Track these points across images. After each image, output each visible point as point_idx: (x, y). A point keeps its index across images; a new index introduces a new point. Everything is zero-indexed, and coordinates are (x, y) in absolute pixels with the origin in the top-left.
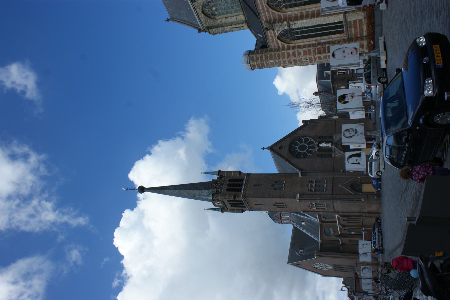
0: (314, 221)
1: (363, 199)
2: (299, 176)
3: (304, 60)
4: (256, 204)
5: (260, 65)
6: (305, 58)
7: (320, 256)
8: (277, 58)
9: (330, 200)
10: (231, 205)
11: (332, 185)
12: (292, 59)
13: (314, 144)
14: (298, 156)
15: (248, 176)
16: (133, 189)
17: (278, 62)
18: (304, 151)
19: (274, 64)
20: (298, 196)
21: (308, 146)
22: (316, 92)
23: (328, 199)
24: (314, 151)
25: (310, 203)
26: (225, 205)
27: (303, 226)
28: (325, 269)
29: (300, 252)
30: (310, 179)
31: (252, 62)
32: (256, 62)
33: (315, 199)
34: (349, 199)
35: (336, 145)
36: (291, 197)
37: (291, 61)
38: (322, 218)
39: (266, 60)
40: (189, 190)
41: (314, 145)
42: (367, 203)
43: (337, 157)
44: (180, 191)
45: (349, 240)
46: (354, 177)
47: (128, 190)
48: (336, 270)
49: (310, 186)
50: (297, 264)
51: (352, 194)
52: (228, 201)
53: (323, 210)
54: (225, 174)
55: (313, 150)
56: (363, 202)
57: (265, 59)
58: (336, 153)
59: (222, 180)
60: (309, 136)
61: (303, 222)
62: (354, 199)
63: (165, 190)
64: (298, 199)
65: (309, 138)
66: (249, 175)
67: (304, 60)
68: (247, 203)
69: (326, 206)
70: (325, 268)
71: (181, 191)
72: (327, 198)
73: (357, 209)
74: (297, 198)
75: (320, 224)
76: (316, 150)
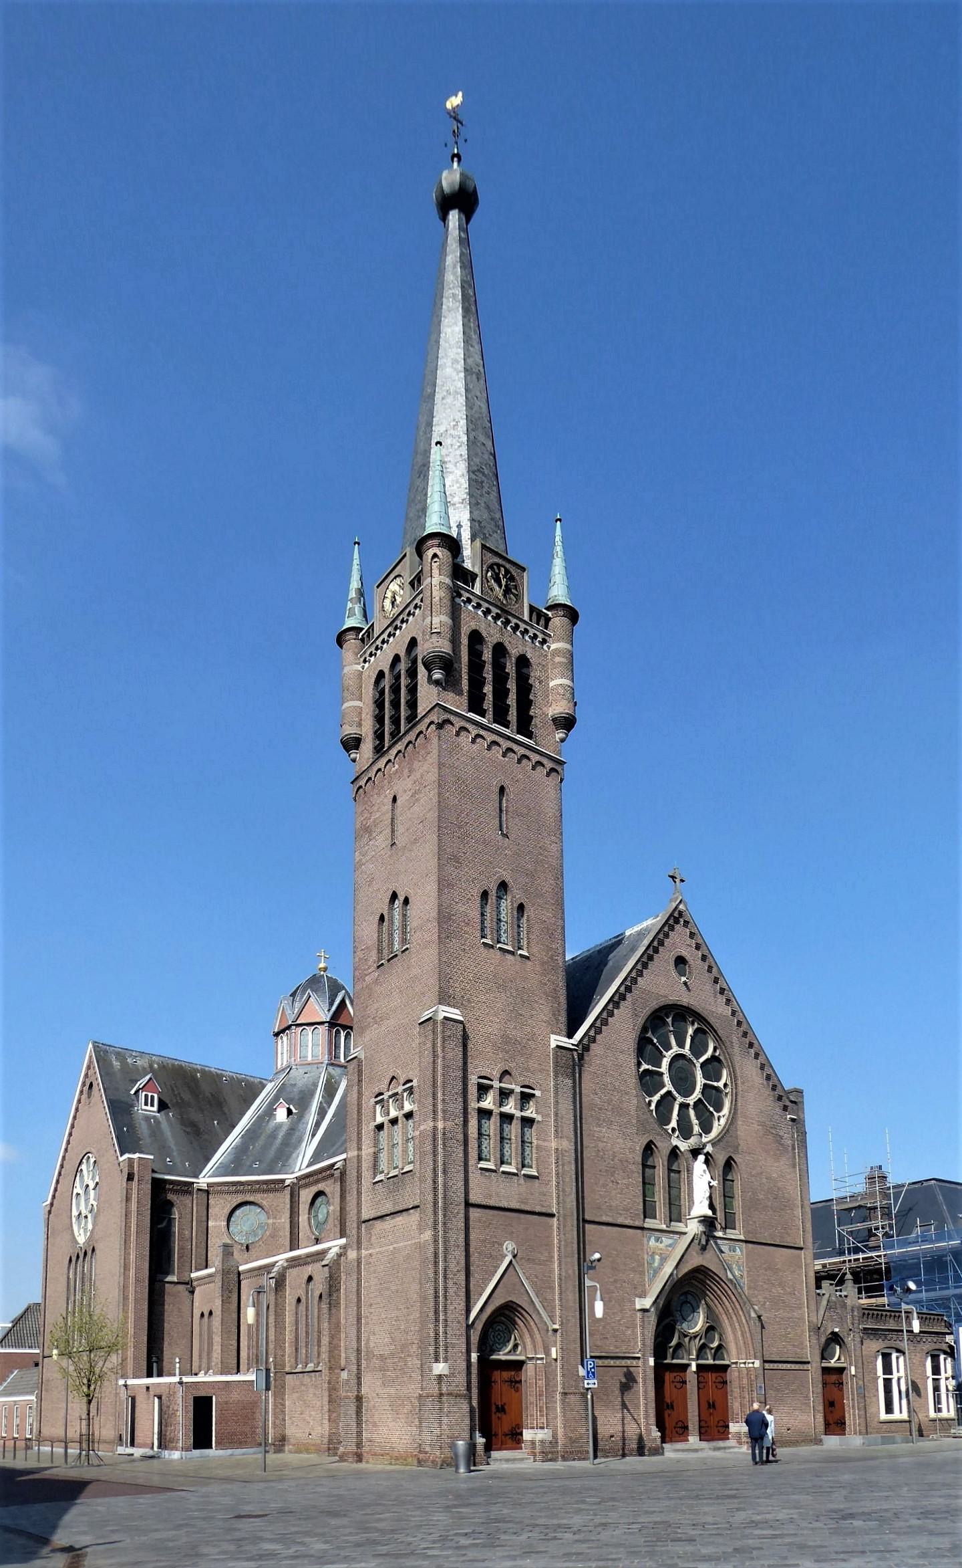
0: (294, 1155)
1: (446, 1372)
4: (395, 799)
7: (130, 1177)
9: (435, 1189)
10: (387, 671)
14: (645, 1048)
15: (549, 765)
18: (666, 1079)
21: (692, 1103)
22: (883, 1178)
23: (440, 1180)
24: (670, 1131)
25: (415, 1083)
26: (385, 636)
27: (270, 1112)
28: (75, 1213)
29: (150, 1094)
30: (537, 1093)
33: (440, 1107)
34: (441, 1293)
35: (704, 1242)
38: (314, 1189)
40: (464, 438)
42: (420, 1396)
43: (645, 1242)
44: (457, 393)
45: (211, 1313)
46: (556, 1327)
49: (503, 1085)
50: (91, 1085)
51: (468, 1311)
53: (366, 1165)
54: (559, 641)
55: (674, 1124)
56: (424, 1370)
58: (666, 1240)
59: (526, 618)
61: (290, 1112)
62: (446, 1320)
63: (460, 318)
64: (436, 1011)
65: (726, 1111)
66: (553, 770)
70: (80, 1214)
71: (462, 400)
72: (445, 1172)
73: (378, 1339)
74: (442, 1007)
75: (283, 1181)
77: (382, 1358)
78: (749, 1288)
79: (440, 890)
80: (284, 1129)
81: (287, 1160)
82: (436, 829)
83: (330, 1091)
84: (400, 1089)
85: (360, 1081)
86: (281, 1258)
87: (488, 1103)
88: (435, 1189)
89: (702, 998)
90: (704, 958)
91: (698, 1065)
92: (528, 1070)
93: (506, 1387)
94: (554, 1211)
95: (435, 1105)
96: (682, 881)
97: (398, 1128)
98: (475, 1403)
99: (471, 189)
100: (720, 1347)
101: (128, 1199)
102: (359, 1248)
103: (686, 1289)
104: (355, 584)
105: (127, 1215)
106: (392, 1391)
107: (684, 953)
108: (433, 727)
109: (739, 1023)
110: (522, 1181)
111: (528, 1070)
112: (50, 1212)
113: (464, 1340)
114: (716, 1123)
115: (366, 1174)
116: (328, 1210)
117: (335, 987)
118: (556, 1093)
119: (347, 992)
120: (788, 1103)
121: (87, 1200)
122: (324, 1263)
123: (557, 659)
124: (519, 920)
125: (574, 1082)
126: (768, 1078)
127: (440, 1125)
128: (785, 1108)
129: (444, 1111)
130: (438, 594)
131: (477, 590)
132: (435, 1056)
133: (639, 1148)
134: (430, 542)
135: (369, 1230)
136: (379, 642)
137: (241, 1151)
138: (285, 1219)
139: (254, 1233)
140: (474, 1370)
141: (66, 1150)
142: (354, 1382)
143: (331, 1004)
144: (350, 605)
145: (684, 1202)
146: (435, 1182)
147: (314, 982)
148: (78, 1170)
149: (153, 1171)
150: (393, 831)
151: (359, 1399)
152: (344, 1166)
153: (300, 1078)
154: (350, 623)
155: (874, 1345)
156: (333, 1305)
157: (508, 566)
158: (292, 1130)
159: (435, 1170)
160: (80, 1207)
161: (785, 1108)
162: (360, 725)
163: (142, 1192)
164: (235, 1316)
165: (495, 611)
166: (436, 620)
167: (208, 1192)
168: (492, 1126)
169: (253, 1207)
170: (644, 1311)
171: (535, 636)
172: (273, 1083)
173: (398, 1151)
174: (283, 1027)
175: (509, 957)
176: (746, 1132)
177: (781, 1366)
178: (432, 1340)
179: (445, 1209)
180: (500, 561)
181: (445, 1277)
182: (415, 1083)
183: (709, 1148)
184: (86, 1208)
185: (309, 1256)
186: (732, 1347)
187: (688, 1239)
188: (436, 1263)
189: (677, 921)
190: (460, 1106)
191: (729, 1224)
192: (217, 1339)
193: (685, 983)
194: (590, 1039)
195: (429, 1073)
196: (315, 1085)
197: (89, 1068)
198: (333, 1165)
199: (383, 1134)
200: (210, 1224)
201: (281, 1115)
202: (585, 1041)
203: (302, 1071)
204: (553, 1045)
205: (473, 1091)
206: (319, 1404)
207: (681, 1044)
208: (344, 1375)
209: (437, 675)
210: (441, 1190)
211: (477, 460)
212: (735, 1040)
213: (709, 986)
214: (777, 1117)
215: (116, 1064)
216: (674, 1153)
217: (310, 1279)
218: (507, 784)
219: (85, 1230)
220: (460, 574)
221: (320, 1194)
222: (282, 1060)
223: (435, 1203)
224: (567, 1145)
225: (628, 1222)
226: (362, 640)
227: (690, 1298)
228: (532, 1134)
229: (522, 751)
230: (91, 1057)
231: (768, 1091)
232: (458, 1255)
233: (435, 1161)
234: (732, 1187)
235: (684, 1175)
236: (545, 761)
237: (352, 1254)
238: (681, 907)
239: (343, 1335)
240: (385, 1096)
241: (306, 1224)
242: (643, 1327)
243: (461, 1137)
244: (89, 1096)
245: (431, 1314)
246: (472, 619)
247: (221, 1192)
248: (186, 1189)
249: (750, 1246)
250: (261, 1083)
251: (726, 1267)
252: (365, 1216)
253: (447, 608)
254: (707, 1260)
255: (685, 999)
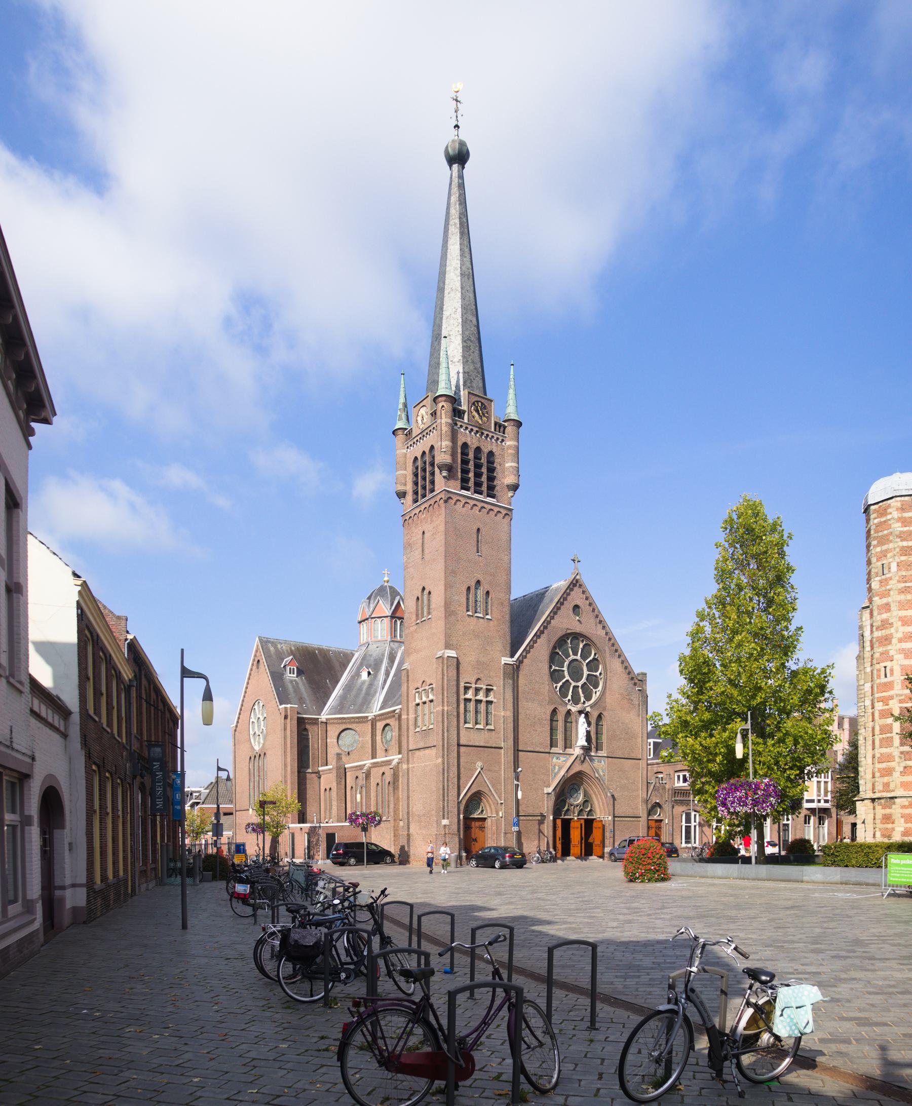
0: (373, 701)
1: (448, 824)
2: (503, 656)
3: (885, 667)
5: (886, 532)
6: (892, 671)
7: (286, 717)
8: (903, 585)
9: (443, 739)
10: (427, 452)
11: (482, 744)
12: (892, 630)
13: (584, 703)
14: (553, 657)
15: (504, 512)
16: (444, 172)
17: (888, 587)
18: (566, 673)
19: (883, 577)
20: (453, 653)
23: (446, 734)
25: (434, 686)
26: (418, 438)
27: (358, 674)
28: (252, 732)
30: (495, 688)
31: (899, 504)
32: (896, 517)
33: (445, 700)
34: (446, 788)
36: (448, 636)
37: (886, 628)
38: (384, 723)
39: (898, 550)
40: (460, 320)
41: (582, 701)
45: (330, 789)
47: (459, 99)
48: (250, 758)
49: (477, 686)
50: (259, 661)
51: (459, 795)
52: (432, 447)
53: (411, 722)
56: (438, 823)
57: (903, 547)
58: (562, 759)
59: (493, 430)
60: (604, 688)
61: (369, 673)
64: (444, 653)
65: (600, 688)
67: (885, 667)
68: (427, 506)
69: (424, 728)
71: (459, 295)
72: (448, 731)
73: (417, 807)
74: (447, 651)
75: (367, 717)
76: (569, 707)
77: (419, 816)
78: (608, 781)
79: (446, 590)
80: (367, 684)
81: (369, 704)
82: (443, 557)
83: (392, 659)
84: (427, 688)
85: (408, 681)
86: (368, 762)
87: (470, 695)
88: (443, 739)
89: (587, 626)
90: (590, 604)
91: (585, 664)
92: (490, 677)
93: (477, 830)
94: (502, 746)
95: (443, 699)
96: (579, 561)
97: (426, 705)
98: (462, 837)
99: (465, 151)
100: (591, 810)
101: (285, 729)
102: (408, 763)
103: (574, 782)
104: (402, 400)
105: (285, 738)
106: (424, 832)
107: (578, 603)
108: (442, 501)
109: (610, 639)
110: (486, 732)
111: (490, 677)
112: (235, 731)
113: (456, 809)
114: (594, 695)
115: (411, 727)
116: (392, 734)
117: (394, 593)
118: (504, 688)
119: (401, 597)
120: (637, 681)
121: (259, 726)
122: (391, 767)
123: (510, 451)
124: (486, 599)
125: (514, 681)
126: (626, 668)
127: (446, 708)
128: (635, 684)
129: (448, 702)
130: (445, 429)
131: (466, 420)
132: (443, 675)
133: (549, 712)
134: (440, 399)
135: (412, 755)
136: (415, 440)
137: (343, 698)
138: (368, 738)
139: (352, 745)
140: (462, 823)
141: (244, 696)
142: (406, 827)
143: (392, 605)
144: (399, 413)
145: (573, 738)
146: (443, 736)
147: (381, 591)
148: (253, 709)
149: (298, 713)
150: (423, 551)
151: (408, 835)
152: (400, 712)
153: (374, 650)
154: (400, 424)
155: (679, 809)
156: (396, 788)
157: (483, 401)
158: (371, 685)
159: (443, 730)
160: (254, 729)
161: (635, 684)
162: (405, 485)
163: (292, 725)
164: (344, 791)
165: (475, 429)
166: (444, 444)
167: (326, 723)
168: (471, 706)
169: (350, 731)
170: (548, 794)
171: (498, 439)
172: (358, 653)
173: (427, 717)
174: (364, 618)
175: (481, 620)
176: (609, 699)
177: (624, 819)
178: (441, 809)
179: (448, 749)
180: (479, 399)
181: (448, 780)
182: (434, 686)
183: (588, 709)
184: (259, 730)
185: (382, 762)
186: (598, 811)
187: (573, 758)
188: (443, 774)
189: (575, 585)
190: (455, 699)
191: (598, 748)
192: (334, 803)
193: (579, 620)
194: (523, 657)
195: (440, 683)
196: (383, 655)
197: (257, 651)
198: (395, 711)
199: (419, 708)
200: (328, 740)
201: (364, 675)
202: (521, 658)
203: (375, 646)
204: (503, 663)
205: (462, 690)
206: (389, 837)
207: (575, 654)
208: (401, 823)
209: (445, 473)
210: (446, 740)
211: (467, 333)
212: (607, 649)
213: (592, 621)
214: (629, 689)
215: (272, 649)
216: (569, 712)
217: (383, 773)
218: (481, 527)
219: (259, 743)
220: (457, 413)
221: (387, 725)
222: (364, 638)
223: (443, 746)
224: (510, 714)
225: (541, 750)
226: (406, 435)
227: (576, 786)
228: (492, 708)
229: (490, 507)
230: (258, 646)
231: (625, 676)
232: (454, 770)
233: (443, 726)
234: (602, 729)
235: (574, 724)
236: (502, 510)
237: (405, 766)
238: (578, 577)
239: (401, 803)
240: (420, 690)
241: (380, 741)
242: (548, 801)
243: (455, 714)
244: (258, 668)
245: (441, 797)
246: (465, 436)
247: (334, 723)
248: (315, 722)
249: (610, 759)
250: (352, 653)
251: (595, 770)
252: (411, 748)
253: (449, 438)
254: (585, 768)
255: (578, 629)
